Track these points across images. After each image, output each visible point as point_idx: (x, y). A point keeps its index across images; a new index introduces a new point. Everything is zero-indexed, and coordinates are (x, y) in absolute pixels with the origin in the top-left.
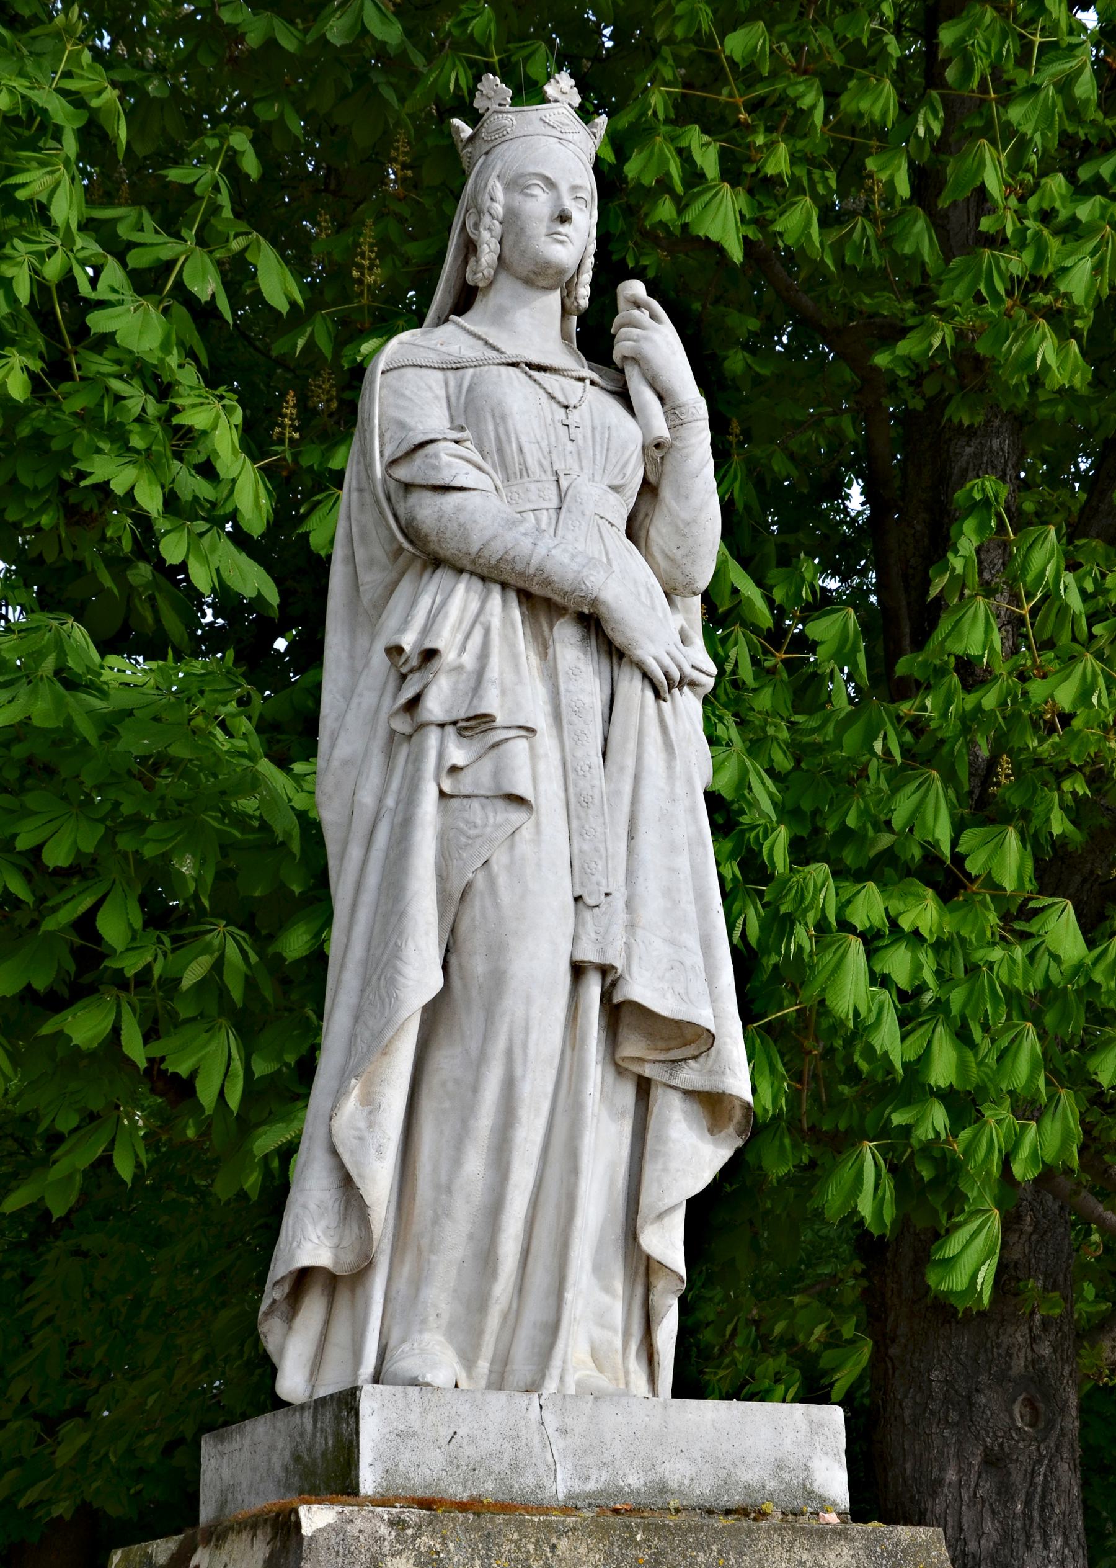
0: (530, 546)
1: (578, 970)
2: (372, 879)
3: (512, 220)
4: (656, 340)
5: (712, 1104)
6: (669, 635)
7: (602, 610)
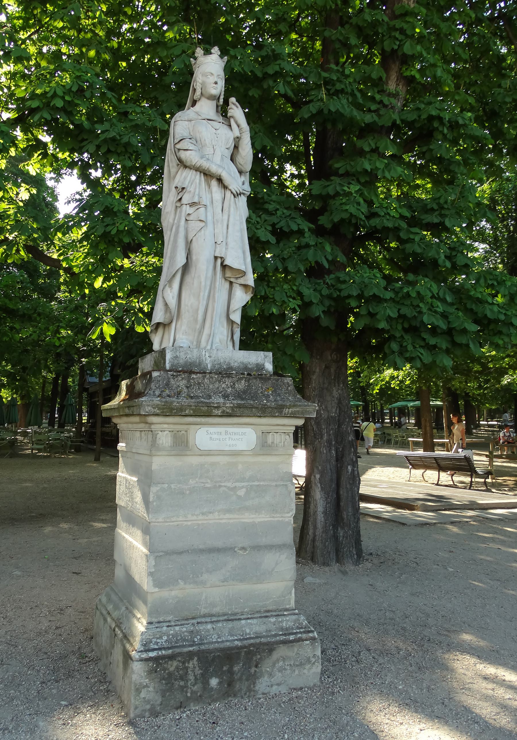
1: (216, 258)
2: (172, 239)
3: (203, 84)
4: (237, 112)
5: (245, 286)
6: (240, 183)
7: (222, 178)
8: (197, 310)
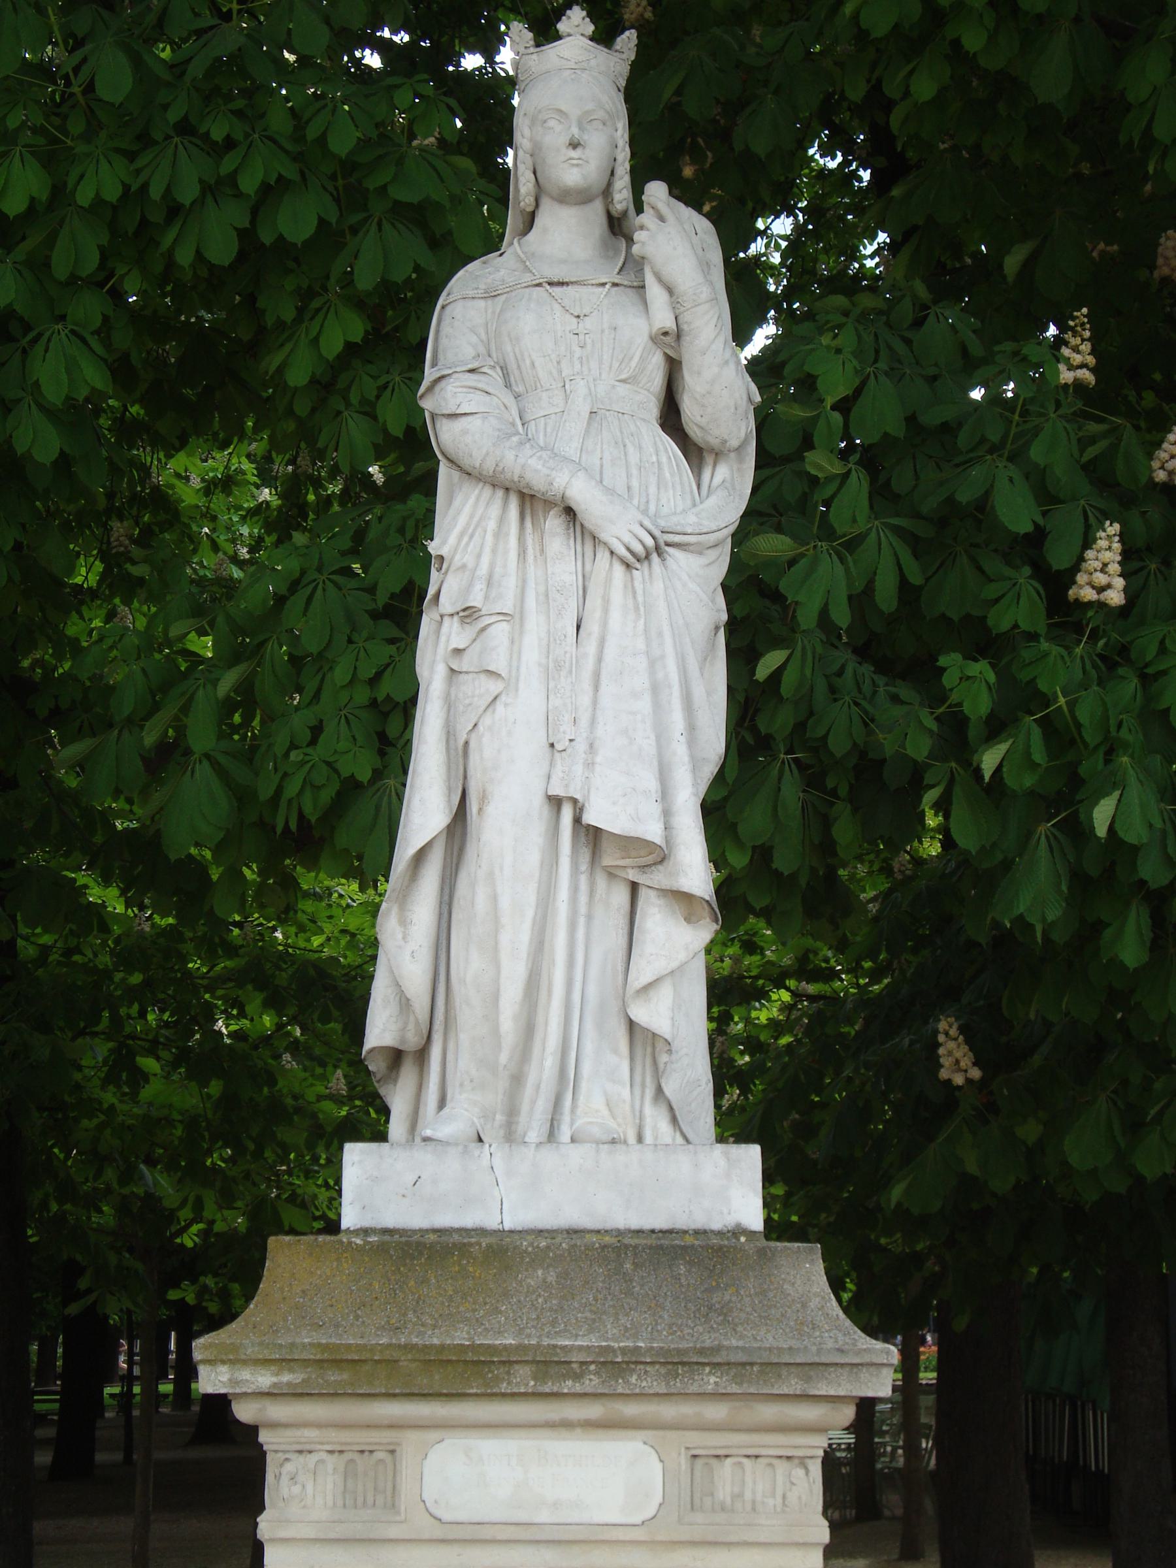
0: (513, 458)
1: (556, 802)
5: (682, 899)
8: (496, 997)
